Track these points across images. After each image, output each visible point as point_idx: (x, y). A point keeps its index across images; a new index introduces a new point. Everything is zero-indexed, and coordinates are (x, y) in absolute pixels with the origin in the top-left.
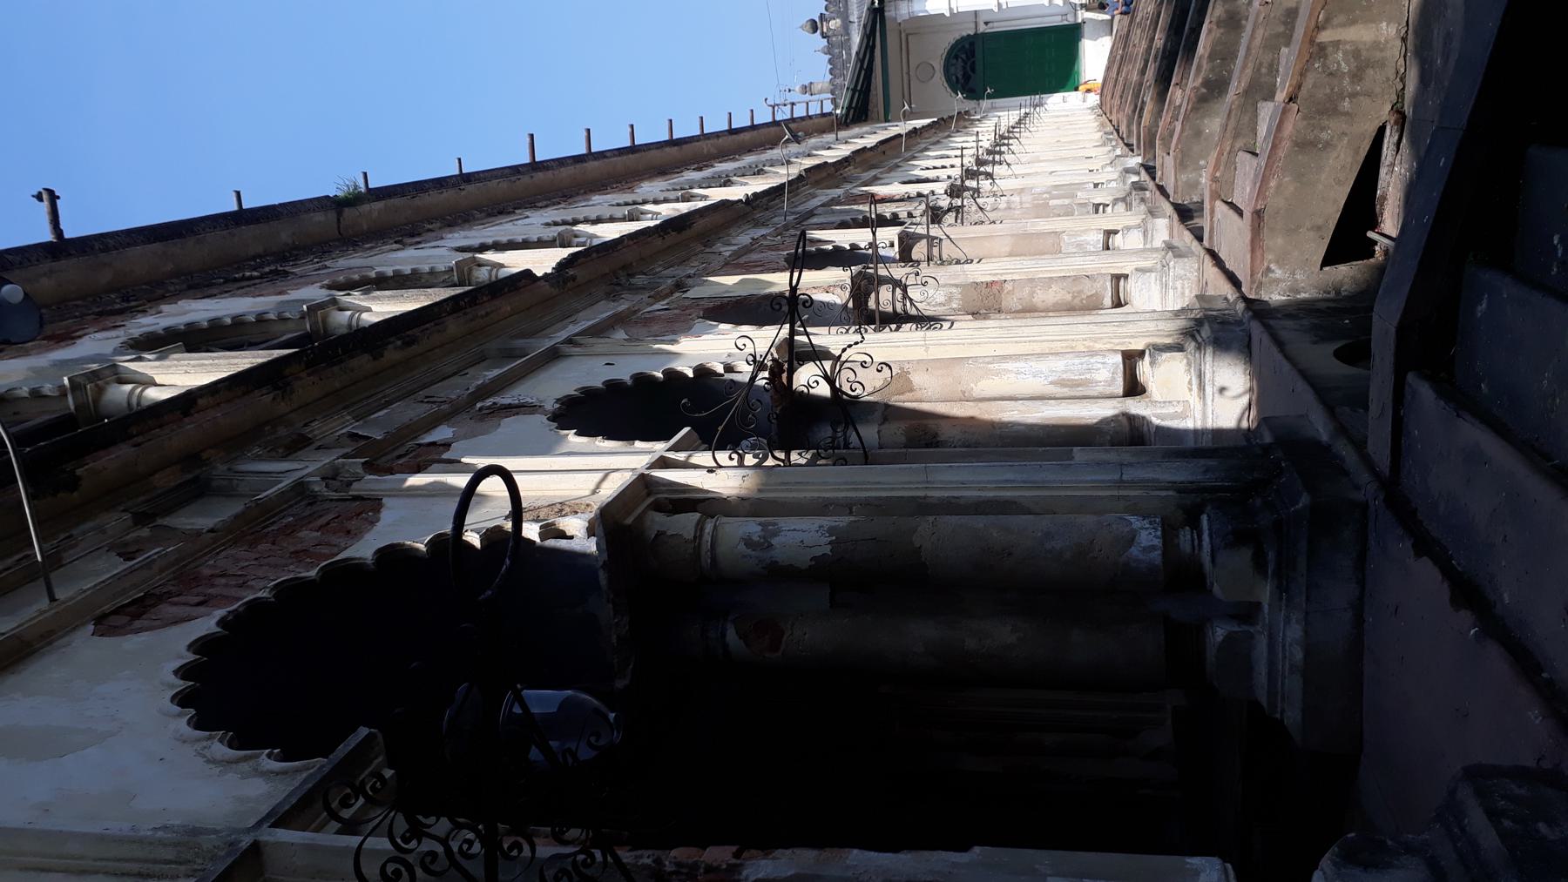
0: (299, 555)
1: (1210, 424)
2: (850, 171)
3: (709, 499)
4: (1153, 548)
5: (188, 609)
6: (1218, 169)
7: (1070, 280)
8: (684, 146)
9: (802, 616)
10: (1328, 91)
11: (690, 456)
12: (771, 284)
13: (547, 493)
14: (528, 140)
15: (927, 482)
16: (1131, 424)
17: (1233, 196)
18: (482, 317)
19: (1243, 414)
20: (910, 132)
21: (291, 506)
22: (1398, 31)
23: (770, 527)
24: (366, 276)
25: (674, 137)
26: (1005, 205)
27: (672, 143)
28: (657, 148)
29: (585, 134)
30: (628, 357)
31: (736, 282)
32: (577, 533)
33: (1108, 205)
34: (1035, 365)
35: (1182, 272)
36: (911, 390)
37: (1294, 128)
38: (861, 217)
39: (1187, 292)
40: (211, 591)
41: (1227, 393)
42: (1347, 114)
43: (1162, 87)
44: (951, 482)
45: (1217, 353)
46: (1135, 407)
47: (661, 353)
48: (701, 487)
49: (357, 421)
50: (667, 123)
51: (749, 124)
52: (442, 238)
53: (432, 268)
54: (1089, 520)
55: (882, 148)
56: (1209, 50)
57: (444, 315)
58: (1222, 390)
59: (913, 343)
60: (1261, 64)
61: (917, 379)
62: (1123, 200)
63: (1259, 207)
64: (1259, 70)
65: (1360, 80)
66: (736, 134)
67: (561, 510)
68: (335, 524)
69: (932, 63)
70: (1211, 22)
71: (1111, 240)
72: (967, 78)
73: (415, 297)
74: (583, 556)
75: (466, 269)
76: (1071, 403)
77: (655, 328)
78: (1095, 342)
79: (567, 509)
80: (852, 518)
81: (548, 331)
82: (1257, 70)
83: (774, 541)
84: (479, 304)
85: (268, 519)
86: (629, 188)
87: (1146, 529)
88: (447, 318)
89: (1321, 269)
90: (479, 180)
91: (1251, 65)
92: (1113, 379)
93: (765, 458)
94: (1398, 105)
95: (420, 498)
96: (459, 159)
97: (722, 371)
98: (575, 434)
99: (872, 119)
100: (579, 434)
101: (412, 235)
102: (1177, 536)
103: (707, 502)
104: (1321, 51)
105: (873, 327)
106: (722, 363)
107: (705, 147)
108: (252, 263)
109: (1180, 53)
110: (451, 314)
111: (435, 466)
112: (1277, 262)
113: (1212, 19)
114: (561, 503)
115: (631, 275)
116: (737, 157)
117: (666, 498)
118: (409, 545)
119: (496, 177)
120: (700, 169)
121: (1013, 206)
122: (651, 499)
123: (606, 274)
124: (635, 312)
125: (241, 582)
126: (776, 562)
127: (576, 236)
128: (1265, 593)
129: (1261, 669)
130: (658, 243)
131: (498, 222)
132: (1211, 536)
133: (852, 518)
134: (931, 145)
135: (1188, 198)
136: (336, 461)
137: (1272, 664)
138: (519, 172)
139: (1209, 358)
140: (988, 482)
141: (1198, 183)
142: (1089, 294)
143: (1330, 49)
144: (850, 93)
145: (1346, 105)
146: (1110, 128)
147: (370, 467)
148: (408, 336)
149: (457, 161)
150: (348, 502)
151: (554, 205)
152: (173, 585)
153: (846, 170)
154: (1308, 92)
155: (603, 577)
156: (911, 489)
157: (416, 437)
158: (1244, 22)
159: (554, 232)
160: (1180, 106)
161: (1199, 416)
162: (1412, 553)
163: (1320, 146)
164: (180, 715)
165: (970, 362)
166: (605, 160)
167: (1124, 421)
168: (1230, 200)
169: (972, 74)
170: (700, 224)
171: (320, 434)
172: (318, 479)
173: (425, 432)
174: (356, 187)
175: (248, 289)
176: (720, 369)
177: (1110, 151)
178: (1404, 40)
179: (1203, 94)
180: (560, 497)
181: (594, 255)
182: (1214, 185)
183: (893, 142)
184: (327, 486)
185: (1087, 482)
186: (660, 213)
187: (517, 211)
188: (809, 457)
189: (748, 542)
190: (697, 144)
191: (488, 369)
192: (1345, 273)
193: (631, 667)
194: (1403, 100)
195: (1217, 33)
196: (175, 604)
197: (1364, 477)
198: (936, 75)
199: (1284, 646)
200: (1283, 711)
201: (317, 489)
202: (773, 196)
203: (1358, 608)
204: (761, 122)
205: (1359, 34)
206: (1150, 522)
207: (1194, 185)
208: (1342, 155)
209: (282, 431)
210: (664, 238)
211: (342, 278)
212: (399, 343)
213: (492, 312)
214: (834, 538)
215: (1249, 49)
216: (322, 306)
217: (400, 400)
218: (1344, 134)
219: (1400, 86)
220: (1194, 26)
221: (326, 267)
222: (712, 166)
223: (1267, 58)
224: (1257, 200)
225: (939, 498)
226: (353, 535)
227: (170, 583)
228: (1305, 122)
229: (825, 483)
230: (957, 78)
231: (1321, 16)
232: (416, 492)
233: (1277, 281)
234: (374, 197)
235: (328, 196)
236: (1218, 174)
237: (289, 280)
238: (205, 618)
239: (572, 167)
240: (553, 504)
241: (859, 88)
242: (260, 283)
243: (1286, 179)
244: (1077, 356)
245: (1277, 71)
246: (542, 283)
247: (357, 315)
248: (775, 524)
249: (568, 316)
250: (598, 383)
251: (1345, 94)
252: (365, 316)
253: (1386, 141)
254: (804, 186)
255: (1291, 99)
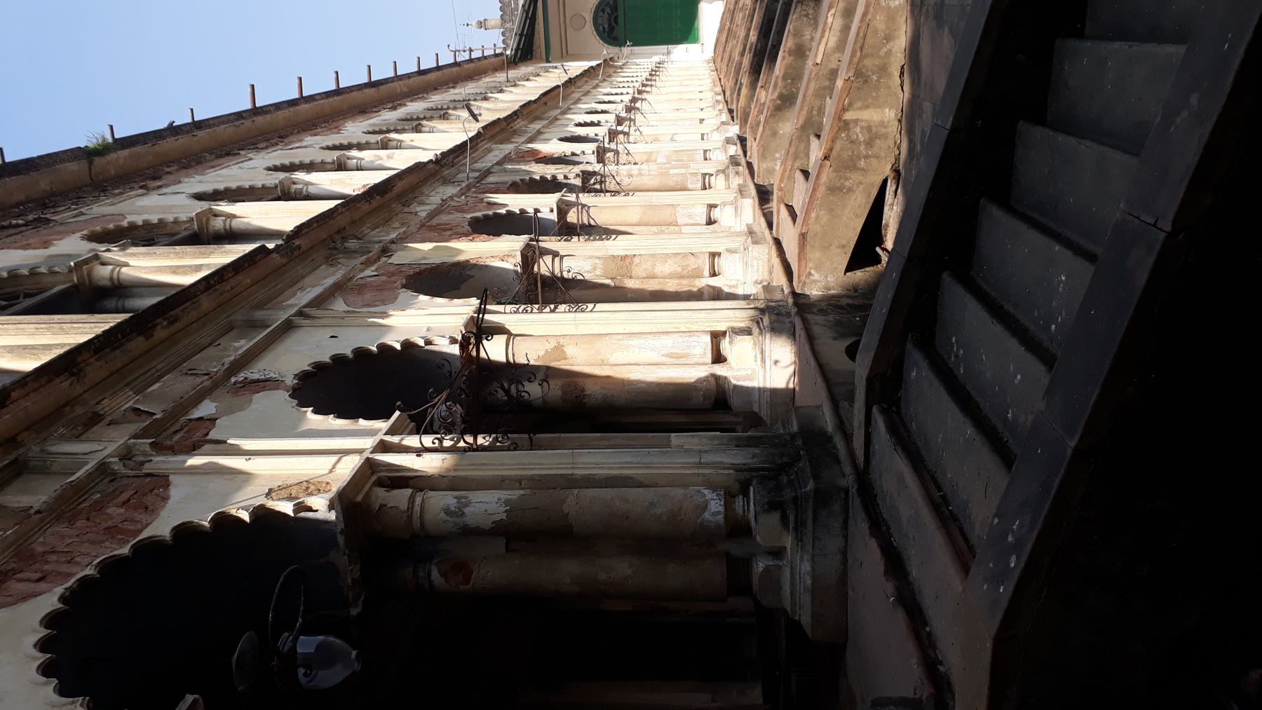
0: (113, 532)
1: (768, 385)
2: (519, 124)
3: (418, 477)
4: (719, 513)
5: (32, 585)
6: (783, 182)
7: (680, 256)
8: (381, 87)
9: (486, 559)
10: (850, 153)
11: (402, 439)
12: (459, 252)
13: (296, 472)
14: (250, 89)
15: (573, 463)
16: (717, 383)
17: (792, 201)
18: (228, 291)
19: (790, 379)
20: (566, 82)
21: (97, 484)
22: (896, 115)
23: (463, 500)
24: (120, 225)
25: (372, 80)
26: (638, 172)
27: (371, 84)
28: (359, 90)
29: (297, 81)
30: (348, 329)
31: (430, 248)
32: (321, 509)
33: (712, 175)
34: (651, 341)
35: (757, 255)
36: (565, 358)
37: (827, 178)
38: (528, 178)
39: (761, 268)
40: (46, 567)
41: (779, 364)
42: (863, 169)
43: (753, 78)
44: (589, 463)
45: (773, 338)
46: (719, 370)
47: (376, 326)
48: (412, 467)
49: (137, 395)
50: (367, 68)
51: (435, 65)
52: (180, 182)
53: (176, 218)
54: (679, 492)
55: (544, 99)
56: (783, 71)
57: (199, 293)
58: (776, 362)
59: (567, 322)
60: (813, 107)
61: (570, 350)
62: (723, 171)
63: (804, 231)
64: (811, 111)
65: (872, 147)
66: (424, 74)
67: (308, 488)
68: (134, 501)
69: (584, 14)
70: (784, 51)
71: (712, 213)
72: (612, 29)
73: (166, 255)
74: (326, 522)
75: (204, 219)
76: (676, 368)
77: (368, 296)
78: (693, 324)
79: (312, 487)
80: (522, 492)
81: (279, 299)
82: (810, 112)
83: (466, 510)
84: (226, 280)
85: (79, 498)
86: (336, 128)
87: (715, 499)
88: (201, 296)
89: (845, 274)
90: (209, 126)
91: (806, 108)
92: (705, 353)
93: (458, 441)
94: (897, 165)
95: (198, 476)
96: (192, 110)
97: (423, 345)
98: (312, 411)
99: (536, 58)
100: (316, 412)
101: (155, 178)
102: (734, 503)
103: (416, 479)
104: (845, 126)
105: (537, 306)
106: (422, 338)
107: (398, 86)
108: (17, 210)
109: (766, 58)
110: (204, 292)
111: (207, 447)
112: (816, 269)
113: (786, 49)
114: (306, 481)
115: (344, 239)
116: (425, 95)
117: (386, 476)
118: (197, 522)
119: (223, 123)
120: (394, 108)
121: (643, 173)
122: (374, 478)
123: (325, 239)
124: (351, 279)
125: (70, 558)
126: (467, 525)
127: (294, 183)
128: (788, 541)
129: (787, 587)
130: (365, 207)
131: (226, 165)
132: (754, 504)
133: (522, 492)
134: (582, 96)
135: (767, 180)
136: (128, 442)
137: (793, 585)
138: (242, 118)
139: (768, 340)
140: (615, 463)
141: (774, 170)
142: (693, 267)
143: (852, 125)
144: (518, 37)
145: (862, 163)
146: (719, 89)
147: (158, 448)
148: (172, 316)
149: (190, 111)
150: (142, 478)
151: (273, 146)
152: (15, 562)
153: (516, 122)
154: (837, 153)
155: (341, 539)
156: (561, 468)
157: (187, 413)
158: (808, 53)
159: (275, 178)
160: (764, 103)
161: (761, 379)
162: (868, 533)
163: (845, 191)
164: (46, 684)
165: (607, 339)
166: (315, 103)
167: (713, 381)
168: (790, 204)
169: (615, 26)
170: (400, 186)
171: (110, 409)
172: (117, 459)
173: (193, 408)
174: (104, 139)
175: (16, 237)
176: (421, 343)
177: (717, 115)
178: (900, 121)
179: (779, 104)
180: (306, 475)
181: (315, 225)
182: (780, 193)
183: (553, 93)
184: (124, 465)
185: (679, 463)
186: (363, 159)
187: (242, 152)
188: (491, 440)
189: (447, 511)
190: (391, 84)
191: (237, 339)
192: (859, 275)
193: (362, 599)
194: (899, 163)
195: (789, 59)
196: (20, 580)
197: (848, 470)
198: (587, 24)
199: (800, 574)
200: (800, 615)
201: (116, 468)
202: (457, 154)
203: (844, 552)
204: (445, 63)
205: (870, 115)
206: (717, 494)
207: (771, 172)
208: (859, 197)
209: (79, 410)
210: (370, 203)
211: (98, 228)
212: (165, 323)
213: (236, 286)
214: (508, 508)
215: (804, 96)
216: (86, 262)
217: (169, 373)
218: (861, 183)
219: (897, 152)
220: (775, 44)
221: (83, 214)
222: (405, 105)
223: (817, 103)
224: (802, 226)
225: (581, 475)
226: (151, 511)
227: (11, 560)
228: (835, 174)
229: (503, 464)
230: (604, 28)
231: (846, 101)
232: (195, 470)
233: (816, 282)
234: (120, 146)
235: (80, 148)
236: (782, 185)
237: (52, 227)
238: (48, 594)
239: (287, 111)
240: (301, 483)
241: (525, 33)
242: (26, 231)
243: (822, 213)
244: (681, 336)
245: (824, 113)
246: (274, 255)
247: (118, 269)
248: (466, 498)
249: (295, 282)
250: (326, 358)
251: (862, 156)
252: (124, 270)
253: (888, 189)
254: (482, 141)
255: (825, 158)
